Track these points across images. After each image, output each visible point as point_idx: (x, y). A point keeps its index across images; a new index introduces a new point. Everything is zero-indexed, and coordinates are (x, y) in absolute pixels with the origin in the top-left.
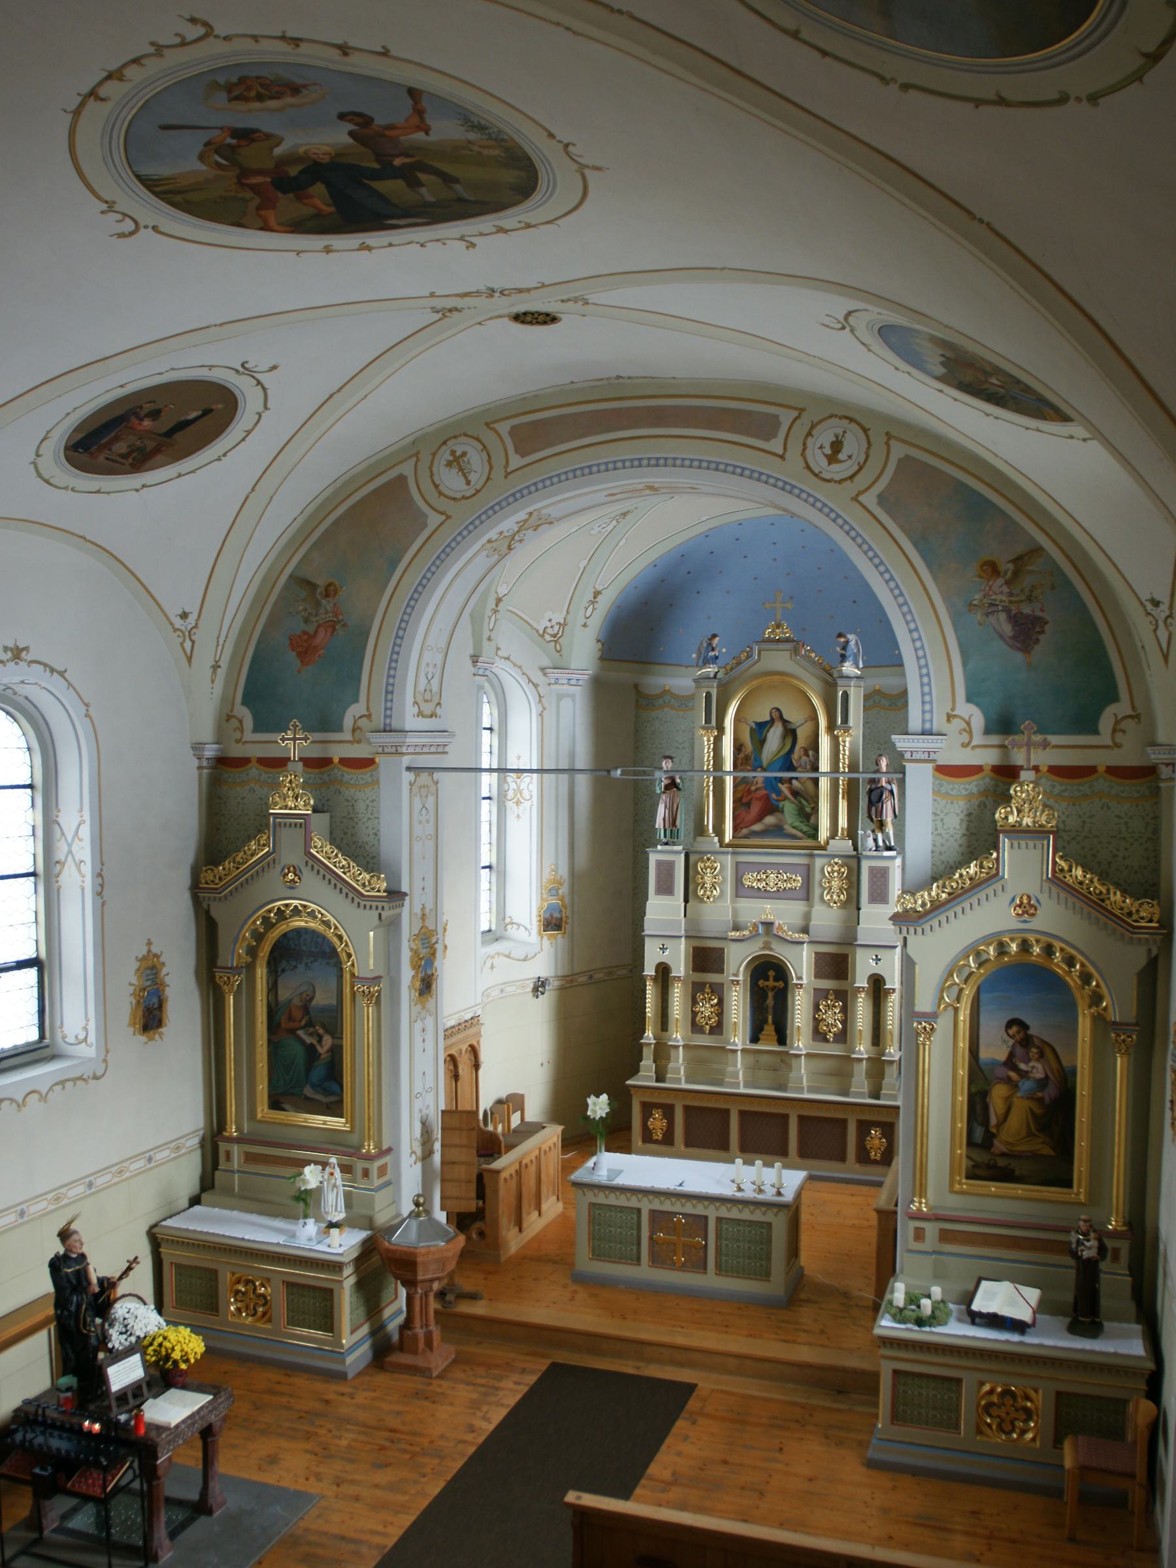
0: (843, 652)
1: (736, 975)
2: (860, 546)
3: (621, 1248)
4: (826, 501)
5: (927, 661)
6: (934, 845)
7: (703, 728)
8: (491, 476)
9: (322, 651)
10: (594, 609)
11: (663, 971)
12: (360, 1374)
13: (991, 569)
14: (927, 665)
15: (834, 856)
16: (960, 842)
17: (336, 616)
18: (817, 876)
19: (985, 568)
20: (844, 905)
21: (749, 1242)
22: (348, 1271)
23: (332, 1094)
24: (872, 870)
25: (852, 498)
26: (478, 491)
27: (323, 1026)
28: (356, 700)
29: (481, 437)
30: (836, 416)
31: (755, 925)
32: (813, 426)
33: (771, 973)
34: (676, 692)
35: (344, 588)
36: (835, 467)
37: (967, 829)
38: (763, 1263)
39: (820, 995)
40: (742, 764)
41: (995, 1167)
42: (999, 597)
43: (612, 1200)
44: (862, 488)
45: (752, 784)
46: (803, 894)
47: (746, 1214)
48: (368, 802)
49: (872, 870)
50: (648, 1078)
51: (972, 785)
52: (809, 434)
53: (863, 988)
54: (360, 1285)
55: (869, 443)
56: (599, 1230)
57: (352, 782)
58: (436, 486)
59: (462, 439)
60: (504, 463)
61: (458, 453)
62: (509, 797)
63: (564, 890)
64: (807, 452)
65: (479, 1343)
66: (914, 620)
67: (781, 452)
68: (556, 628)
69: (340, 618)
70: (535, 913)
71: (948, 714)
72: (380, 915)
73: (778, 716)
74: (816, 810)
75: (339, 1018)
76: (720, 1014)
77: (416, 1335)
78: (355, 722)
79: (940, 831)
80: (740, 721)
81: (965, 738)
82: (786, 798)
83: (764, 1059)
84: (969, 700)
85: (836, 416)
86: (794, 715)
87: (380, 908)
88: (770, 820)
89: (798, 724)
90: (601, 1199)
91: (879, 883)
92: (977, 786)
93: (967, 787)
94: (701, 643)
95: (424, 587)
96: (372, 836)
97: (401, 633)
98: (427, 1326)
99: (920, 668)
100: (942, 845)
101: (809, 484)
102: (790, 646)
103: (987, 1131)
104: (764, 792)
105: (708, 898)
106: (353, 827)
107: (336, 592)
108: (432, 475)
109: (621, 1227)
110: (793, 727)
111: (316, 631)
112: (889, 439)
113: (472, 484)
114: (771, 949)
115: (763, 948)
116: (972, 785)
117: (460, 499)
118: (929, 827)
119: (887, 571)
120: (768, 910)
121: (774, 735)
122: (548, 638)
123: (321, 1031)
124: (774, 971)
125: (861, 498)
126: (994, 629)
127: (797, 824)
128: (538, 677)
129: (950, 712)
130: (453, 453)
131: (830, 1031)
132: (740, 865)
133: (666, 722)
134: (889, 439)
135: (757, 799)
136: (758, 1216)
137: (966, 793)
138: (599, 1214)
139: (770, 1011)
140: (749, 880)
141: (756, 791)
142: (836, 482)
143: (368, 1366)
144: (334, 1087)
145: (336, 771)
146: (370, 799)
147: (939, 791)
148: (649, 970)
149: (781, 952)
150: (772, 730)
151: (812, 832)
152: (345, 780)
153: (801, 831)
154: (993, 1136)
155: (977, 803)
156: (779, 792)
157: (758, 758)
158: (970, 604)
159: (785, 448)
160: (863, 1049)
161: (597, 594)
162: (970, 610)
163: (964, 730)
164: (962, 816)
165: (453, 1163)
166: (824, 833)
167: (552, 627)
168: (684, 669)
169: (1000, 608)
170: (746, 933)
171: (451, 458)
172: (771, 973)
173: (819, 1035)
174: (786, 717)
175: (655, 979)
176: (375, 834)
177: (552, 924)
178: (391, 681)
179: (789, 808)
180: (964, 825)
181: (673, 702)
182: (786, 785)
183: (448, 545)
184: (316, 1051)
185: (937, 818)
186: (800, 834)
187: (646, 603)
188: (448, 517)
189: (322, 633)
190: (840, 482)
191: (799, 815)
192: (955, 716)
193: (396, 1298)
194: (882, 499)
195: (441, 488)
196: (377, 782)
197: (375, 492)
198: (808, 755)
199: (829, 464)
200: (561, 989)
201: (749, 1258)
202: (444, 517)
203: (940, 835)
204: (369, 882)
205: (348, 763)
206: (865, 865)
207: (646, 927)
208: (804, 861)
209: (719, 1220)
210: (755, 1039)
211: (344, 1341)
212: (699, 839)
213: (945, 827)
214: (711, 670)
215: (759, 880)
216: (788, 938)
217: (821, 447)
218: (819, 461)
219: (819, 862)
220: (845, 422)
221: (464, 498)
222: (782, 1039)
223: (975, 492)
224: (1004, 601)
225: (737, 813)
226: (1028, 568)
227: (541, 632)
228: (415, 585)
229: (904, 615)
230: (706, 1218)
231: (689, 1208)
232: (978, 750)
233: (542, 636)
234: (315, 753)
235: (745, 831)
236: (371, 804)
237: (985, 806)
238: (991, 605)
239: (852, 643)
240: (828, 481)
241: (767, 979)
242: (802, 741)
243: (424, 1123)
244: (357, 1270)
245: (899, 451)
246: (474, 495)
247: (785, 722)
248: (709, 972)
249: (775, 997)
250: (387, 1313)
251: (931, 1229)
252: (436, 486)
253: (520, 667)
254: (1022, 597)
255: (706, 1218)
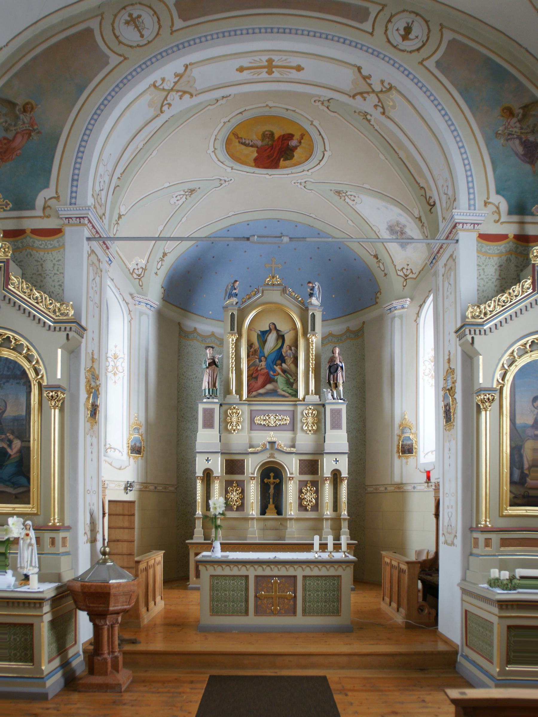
0: (312, 292)
1: (253, 474)
2: (425, 93)
3: (233, 606)
4: (402, 64)
5: (470, 167)
6: (479, 286)
7: (229, 333)
8: (160, 33)
9: (19, 152)
10: (162, 265)
11: (208, 475)
12: (57, 695)
13: (509, 112)
14: (470, 170)
15: (309, 405)
16: (495, 284)
17: (32, 126)
18: (299, 416)
19: (505, 111)
20: (316, 432)
21: (325, 591)
22: (46, 608)
23: (21, 486)
24: (332, 411)
25: (419, 63)
26: (149, 42)
27: (13, 433)
28: (47, 186)
29: (153, 6)
30: (407, 11)
31: (264, 445)
32: (392, 16)
33: (272, 475)
34: (200, 332)
35: (40, 106)
36: (406, 43)
37: (500, 276)
38: (335, 604)
39: (303, 484)
40: (252, 355)
41: (528, 496)
42: (514, 130)
43: (227, 571)
44: (425, 57)
45: (258, 366)
46: (290, 427)
47: (324, 572)
48: (54, 262)
49: (332, 411)
50: (199, 538)
51: (502, 247)
52: (389, 21)
53: (329, 477)
54: (53, 624)
55: (429, 29)
56: (217, 594)
57: (42, 247)
58: (117, 37)
59: (138, 6)
60: (170, 24)
61: (135, 16)
62: (109, 370)
63: (142, 430)
64: (388, 32)
65: (146, 671)
66: (461, 141)
67: (371, 31)
68: (140, 270)
69: (35, 127)
70: (125, 441)
71: (485, 201)
72: (68, 335)
73: (274, 327)
74: (296, 380)
75: (28, 427)
76: (242, 499)
77: (105, 659)
78: (46, 202)
79: (482, 276)
80: (251, 330)
81: (496, 217)
82: (279, 374)
83: (270, 524)
84: (498, 192)
85: (407, 11)
86: (283, 327)
87: (68, 329)
88: (269, 387)
89: (286, 332)
90: (219, 571)
91: (336, 418)
92: (505, 247)
93: (499, 248)
94: (228, 286)
95: (105, 106)
96: (57, 287)
97: (86, 138)
98: (113, 652)
99: (466, 171)
100: (484, 286)
101: (389, 52)
102: (280, 288)
103: (522, 472)
104: (266, 371)
105: (234, 430)
106: (42, 281)
107: (32, 109)
108: (113, 29)
109: (233, 591)
110: (282, 334)
111: (15, 137)
112: (442, 28)
113: (145, 37)
114: (274, 458)
115: (270, 457)
116: (502, 247)
117: (135, 47)
118: (475, 275)
119: (443, 109)
120: (272, 436)
121: (272, 338)
122: (135, 276)
123: (11, 437)
124: (274, 473)
125: (425, 63)
126: (512, 149)
127: (285, 389)
128: (129, 299)
129: (486, 199)
130: (130, 15)
131: (309, 505)
132: (253, 412)
133: (194, 348)
134: (442, 28)
135: (261, 374)
136: (332, 572)
137: (499, 252)
138: (217, 583)
139: (271, 497)
140: (257, 420)
141: (261, 370)
142: (408, 52)
143: (62, 690)
144: (23, 480)
145: (28, 238)
146: (57, 259)
147: (481, 250)
148: (199, 473)
149: (280, 458)
150: (270, 335)
151: (294, 393)
152: (35, 245)
153: (288, 393)
154: (527, 475)
155: (505, 258)
156: (274, 371)
157: (262, 351)
158: (497, 133)
159: (373, 29)
160: (328, 512)
161: (165, 254)
162: (496, 137)
163: (495, 212)
164: (496, 267)
165: (118, 541)
166: (301, 393)
167: (138, 269)
168: (205, 319)
169: (515, 136)
170: (259, 449)
171: (129, 19)
172: (272, 475)
173: (302, 507)
174: (278, 328)
175: (202, 480)
176: (60, 286)
177: (136, 450)
178: (77, 172)
179: (281, 379)
180: (498, 273)
181: (198, 338)
182: (278, 367)
183: (126, 78)
184: (7, 452)
185: (480, 268)
186: (287, 395)
187: (189, 272)
188: (126, 59)
189: (19, 139)
190: (411, 52)
191: (287, 383)
192: (490, 203)
193: (76, 643)
194: (438, 64)
195: (120, 38)
196: (63, 246)
197: (67, 39)
198: (291, 350)
199: (403, 40)
200: (140, 491)
201: (325, 602)
202: (122, 58)
203: (482, 279)
204: (59, 309)
205: (37, 232)
206: (328, 408)
207: (197, 447)
208: (291, 408)
209: (305, 577)
210: (263, 512)
211: (43, 668)
212: (228, 396)
213: (486, 274)
214: (234, 300)
215: (264, 420)
216: (284, 451)
217: (397, 30)
218: (396, 39)
219: (300, 409)
220: (413, 16)
221: (138, 46)
222: (279, 513)
223: (498, 65)
224: (518, 132)
225: (250, 383)
226: (532, 113)
227: (131, 271)
228: (99, 104)
229: (455, 137)
230: (295, 577)
231: (283, 571)
232: (504, 225)
233: (132, 274)
234: (11, 225)
235: (254, 393)
236: (57, 263)
237: (510, 261)
238: (509, 134)
239: (316, 287)
240: (403, 51)
241: (269, 478)
242: (288, 342)
243: (92, 515)
244: (53, 607)
245: (448, 36)
246: (146, 45)
247: (278, 331)
248: (235, 474)
249: (274, 488)
250: (71, 653)
251: (495, 538)
252: (117, 37)
253: (119, 289)
254: (529, 130)
255: (295, 577)
